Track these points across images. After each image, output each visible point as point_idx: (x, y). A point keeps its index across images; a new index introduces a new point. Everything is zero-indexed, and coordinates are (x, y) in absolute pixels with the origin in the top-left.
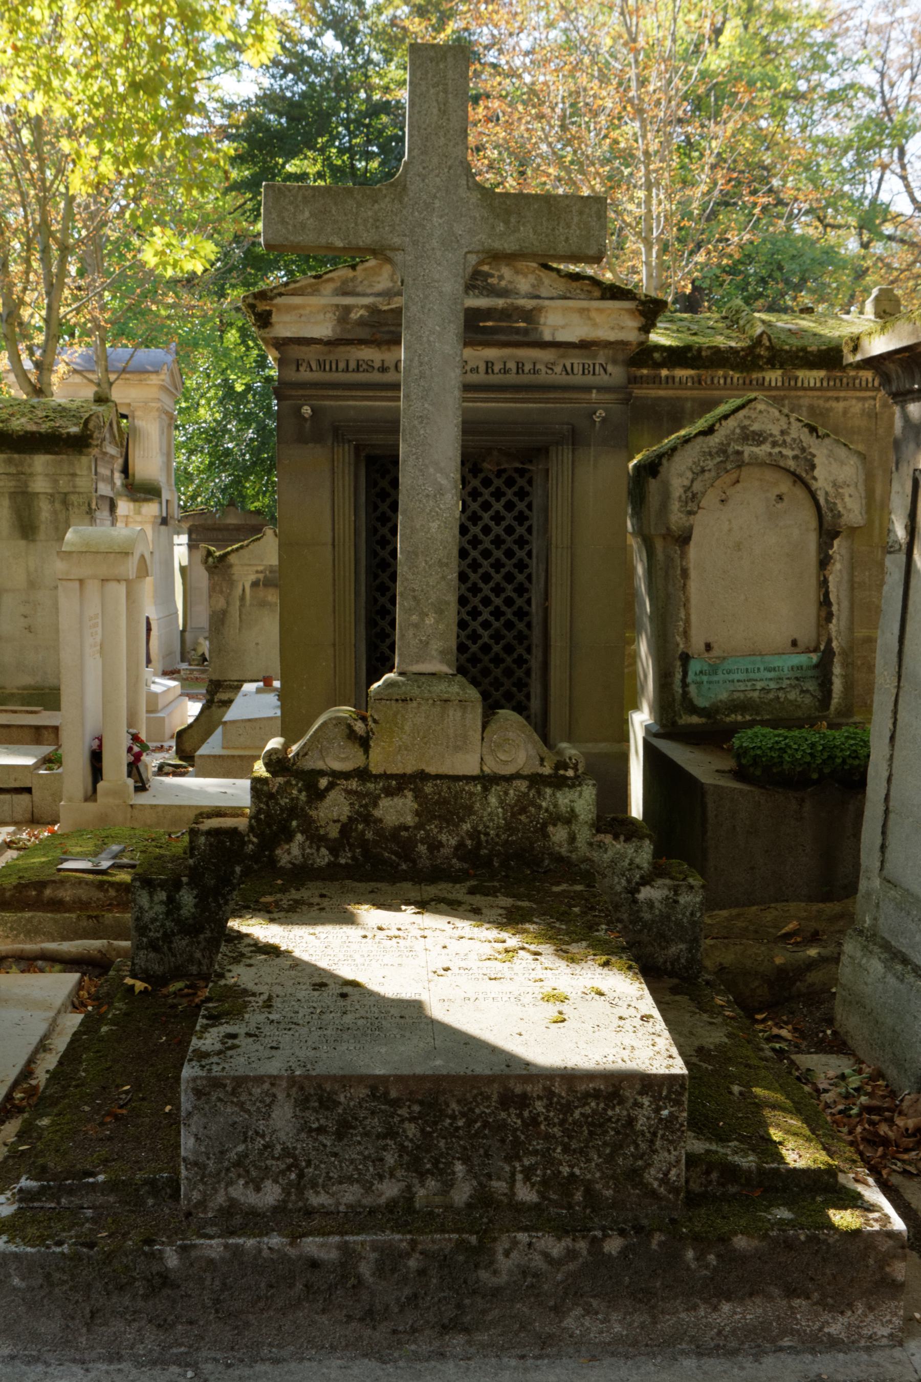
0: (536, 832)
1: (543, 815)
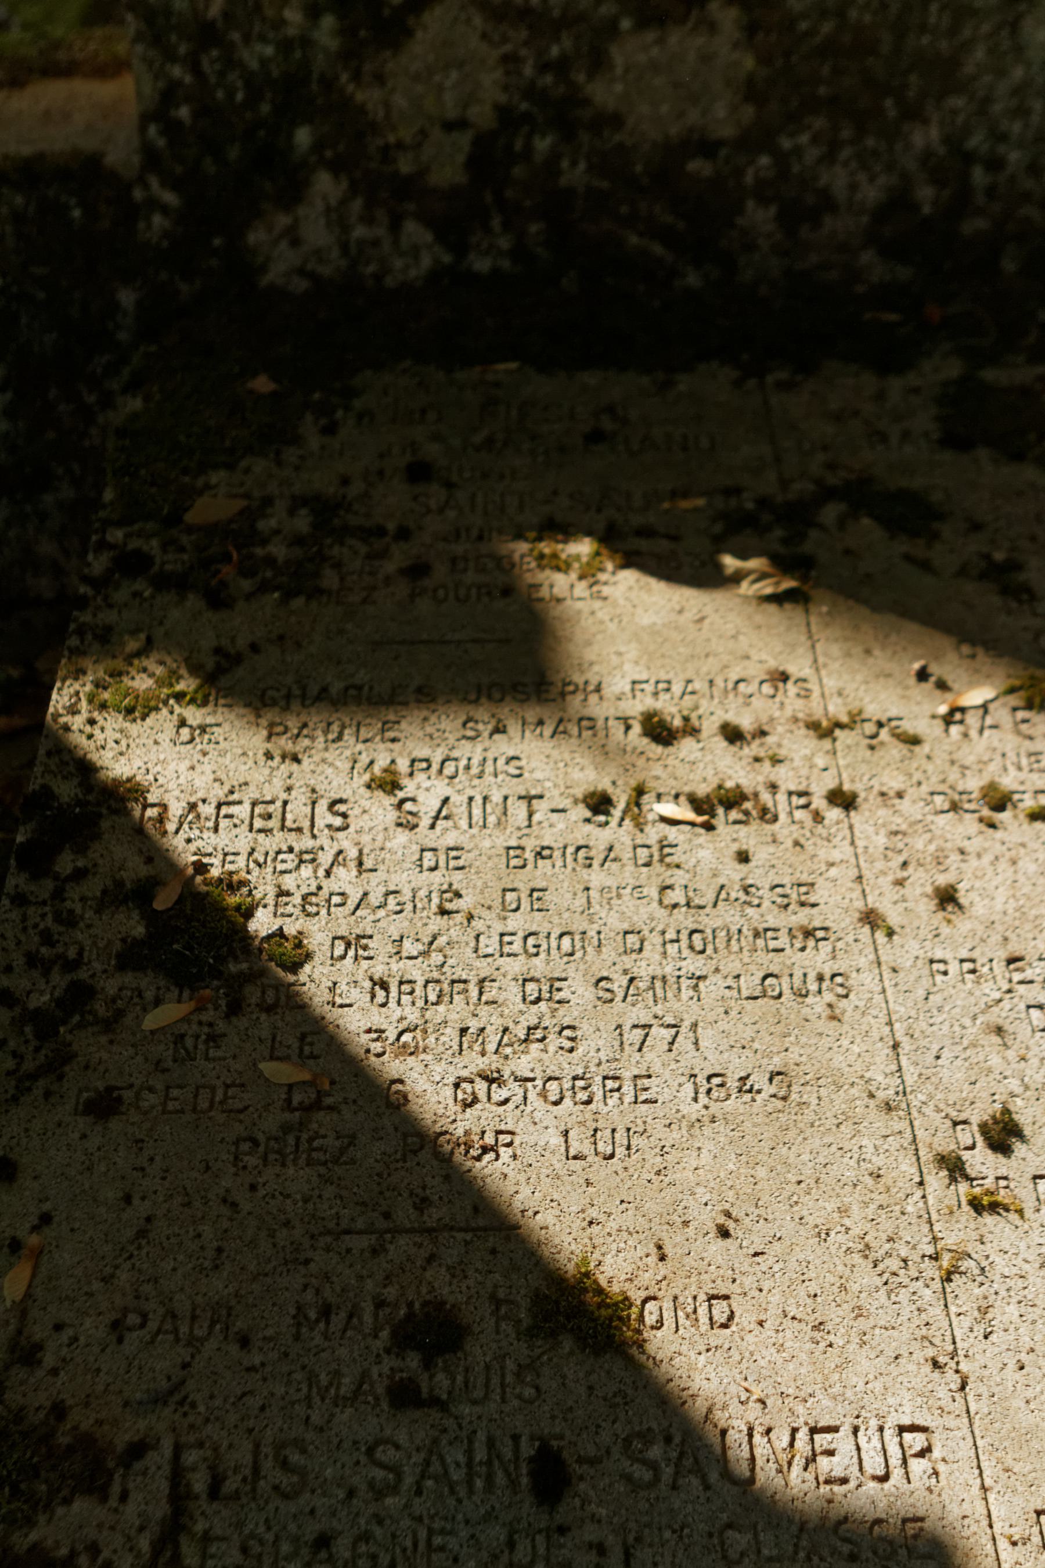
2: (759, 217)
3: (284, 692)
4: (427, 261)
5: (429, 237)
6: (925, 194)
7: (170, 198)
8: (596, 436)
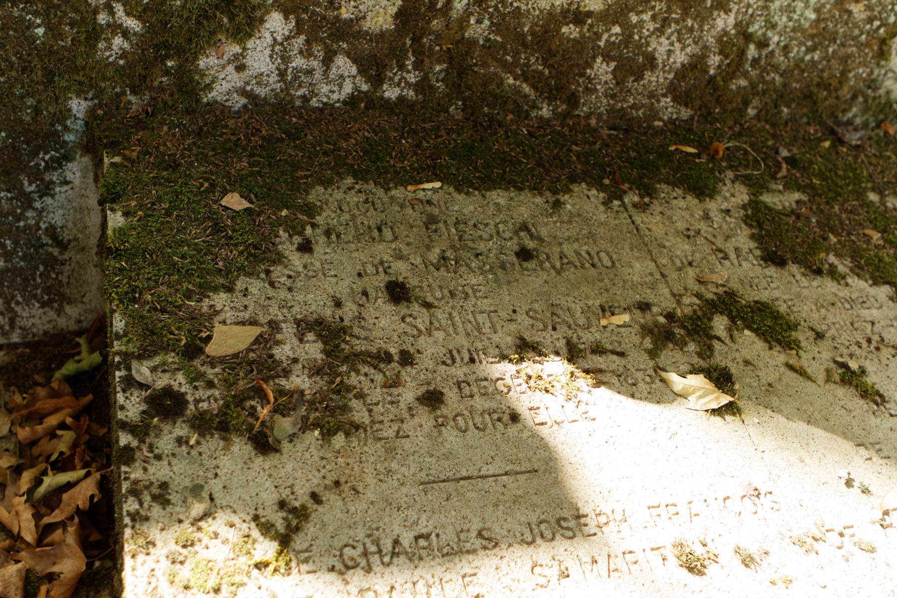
2: (602, 70)
3: (360, 549)
4: (348, 88)
5: (354, 70)
6: (714, 60)
7: (133, 24)
8: (524, 254)
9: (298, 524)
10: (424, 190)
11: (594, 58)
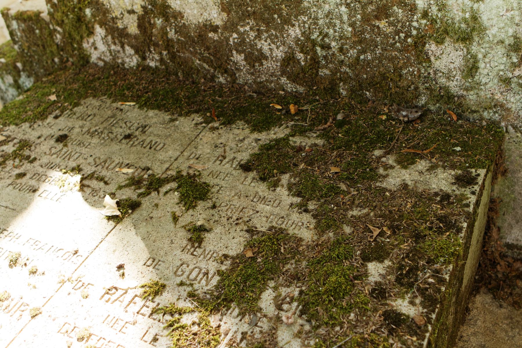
0: (405, 49)
1: (418, 22)
9: (312, 324)
10: (126, 105)
11: (231, 51)
